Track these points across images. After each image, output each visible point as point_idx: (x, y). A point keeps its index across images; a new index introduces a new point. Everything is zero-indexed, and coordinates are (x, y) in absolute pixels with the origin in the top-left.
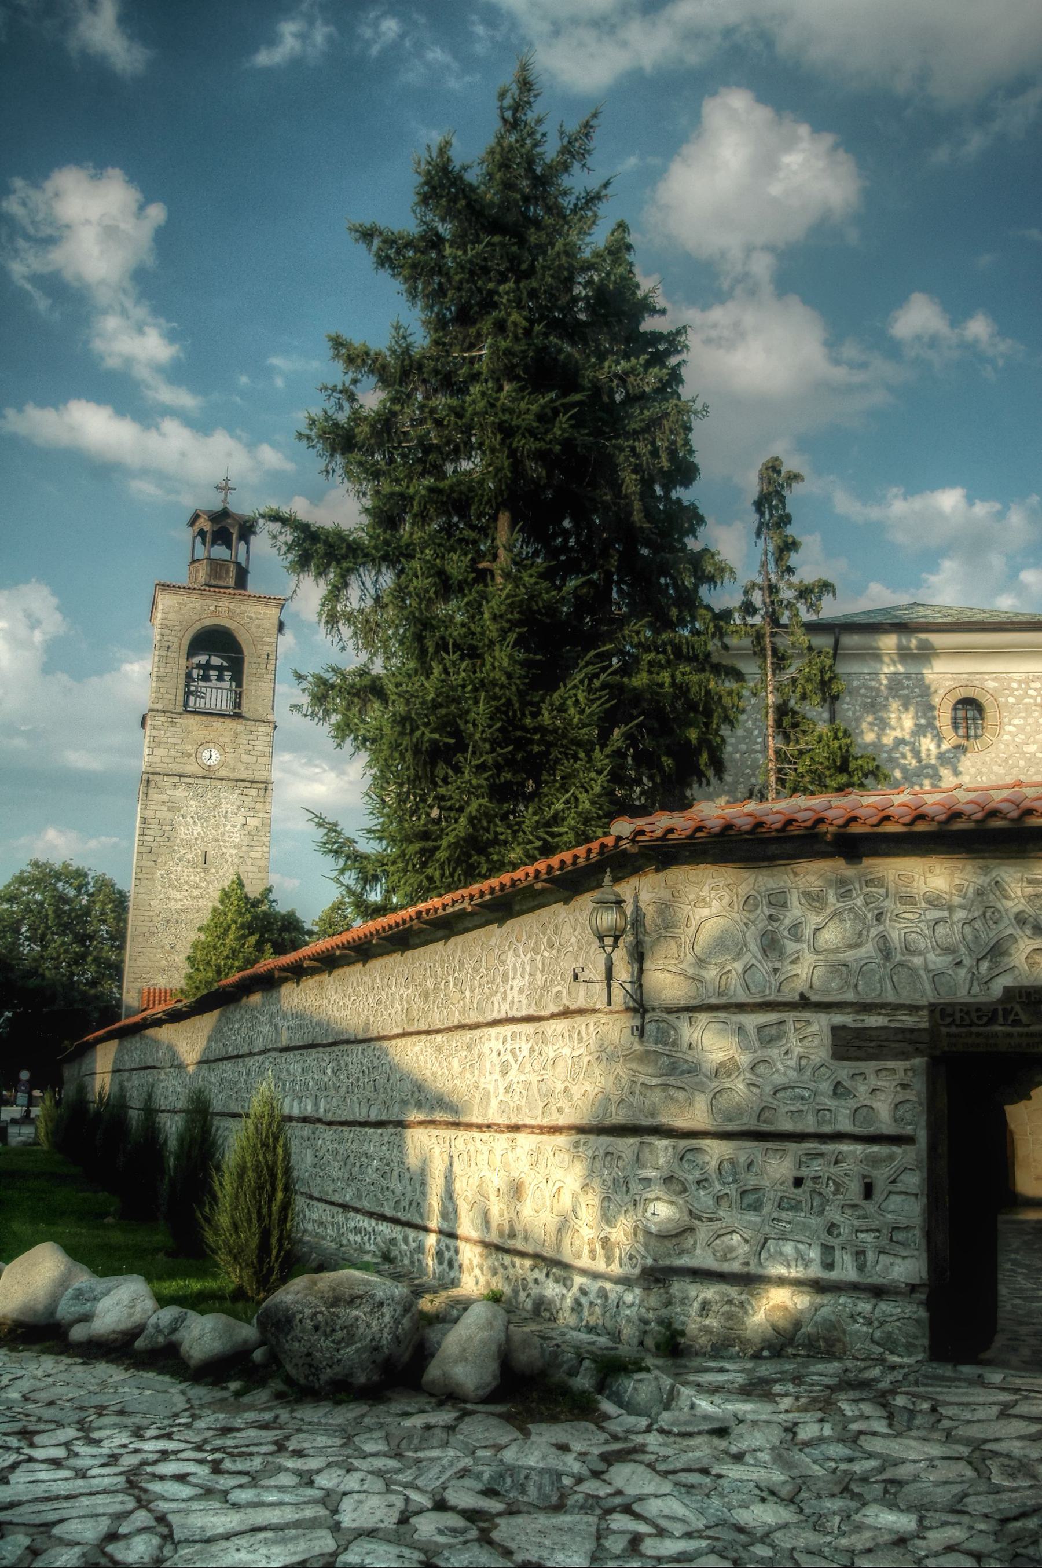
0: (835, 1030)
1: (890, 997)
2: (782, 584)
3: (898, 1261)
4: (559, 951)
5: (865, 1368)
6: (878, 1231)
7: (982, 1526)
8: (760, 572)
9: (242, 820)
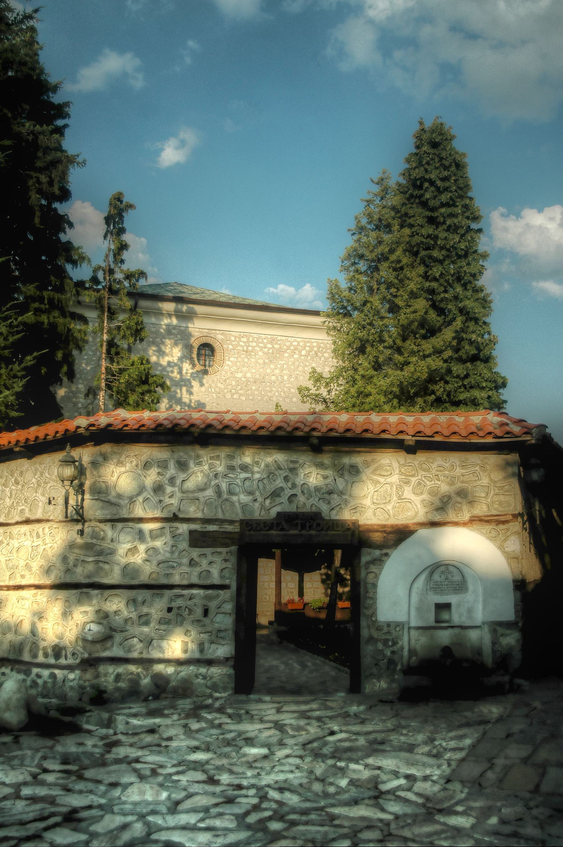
1: (220, 516)
2: (117, 269)
3: (220, 647)
4: (23, 486)
5: (204, 700)
6: (210, 632)
7: (297, 747)
8: (105, 261)
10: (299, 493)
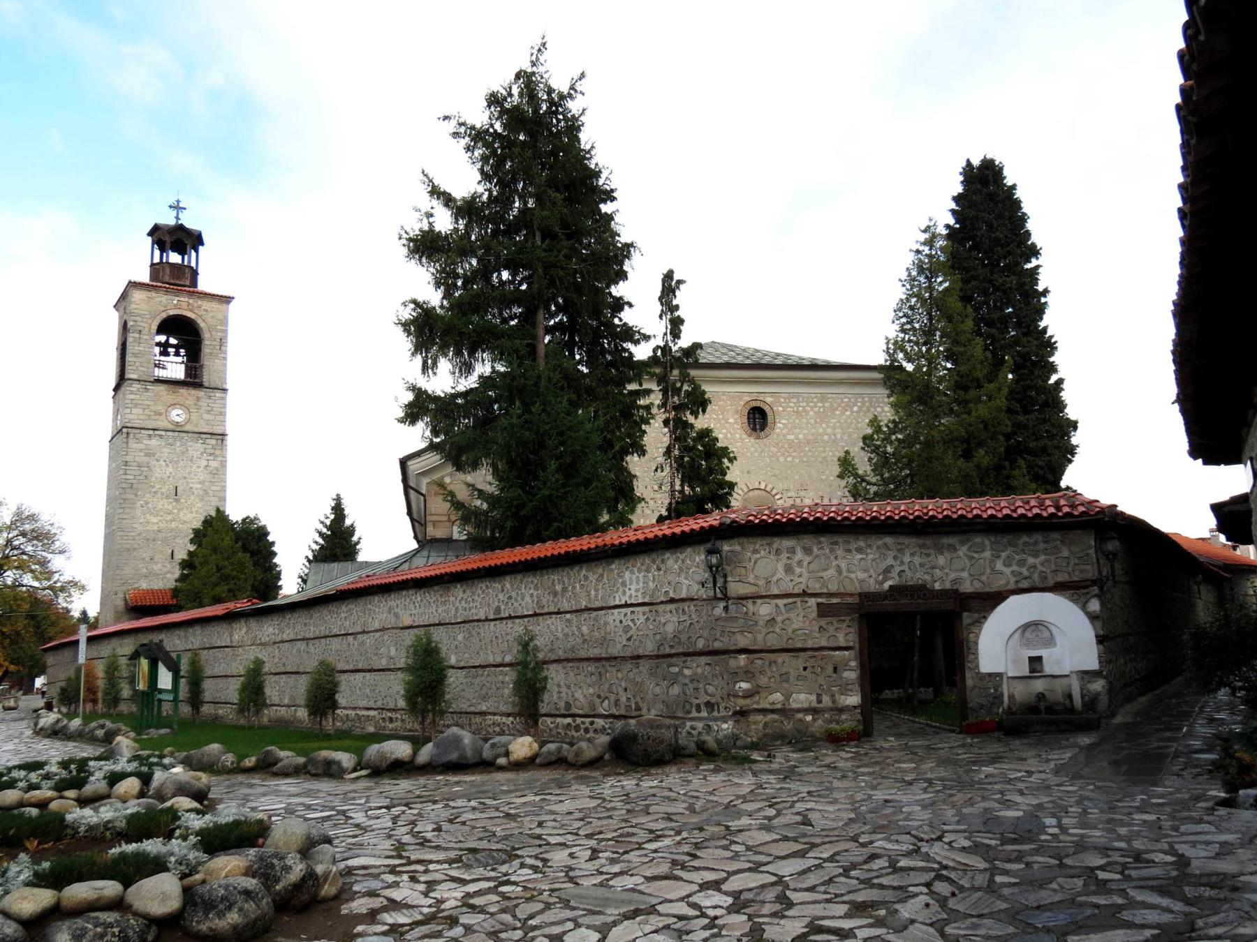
0: (818, 604)
1: (842, 590)
9: (205, 463)
10: (907, 569)
